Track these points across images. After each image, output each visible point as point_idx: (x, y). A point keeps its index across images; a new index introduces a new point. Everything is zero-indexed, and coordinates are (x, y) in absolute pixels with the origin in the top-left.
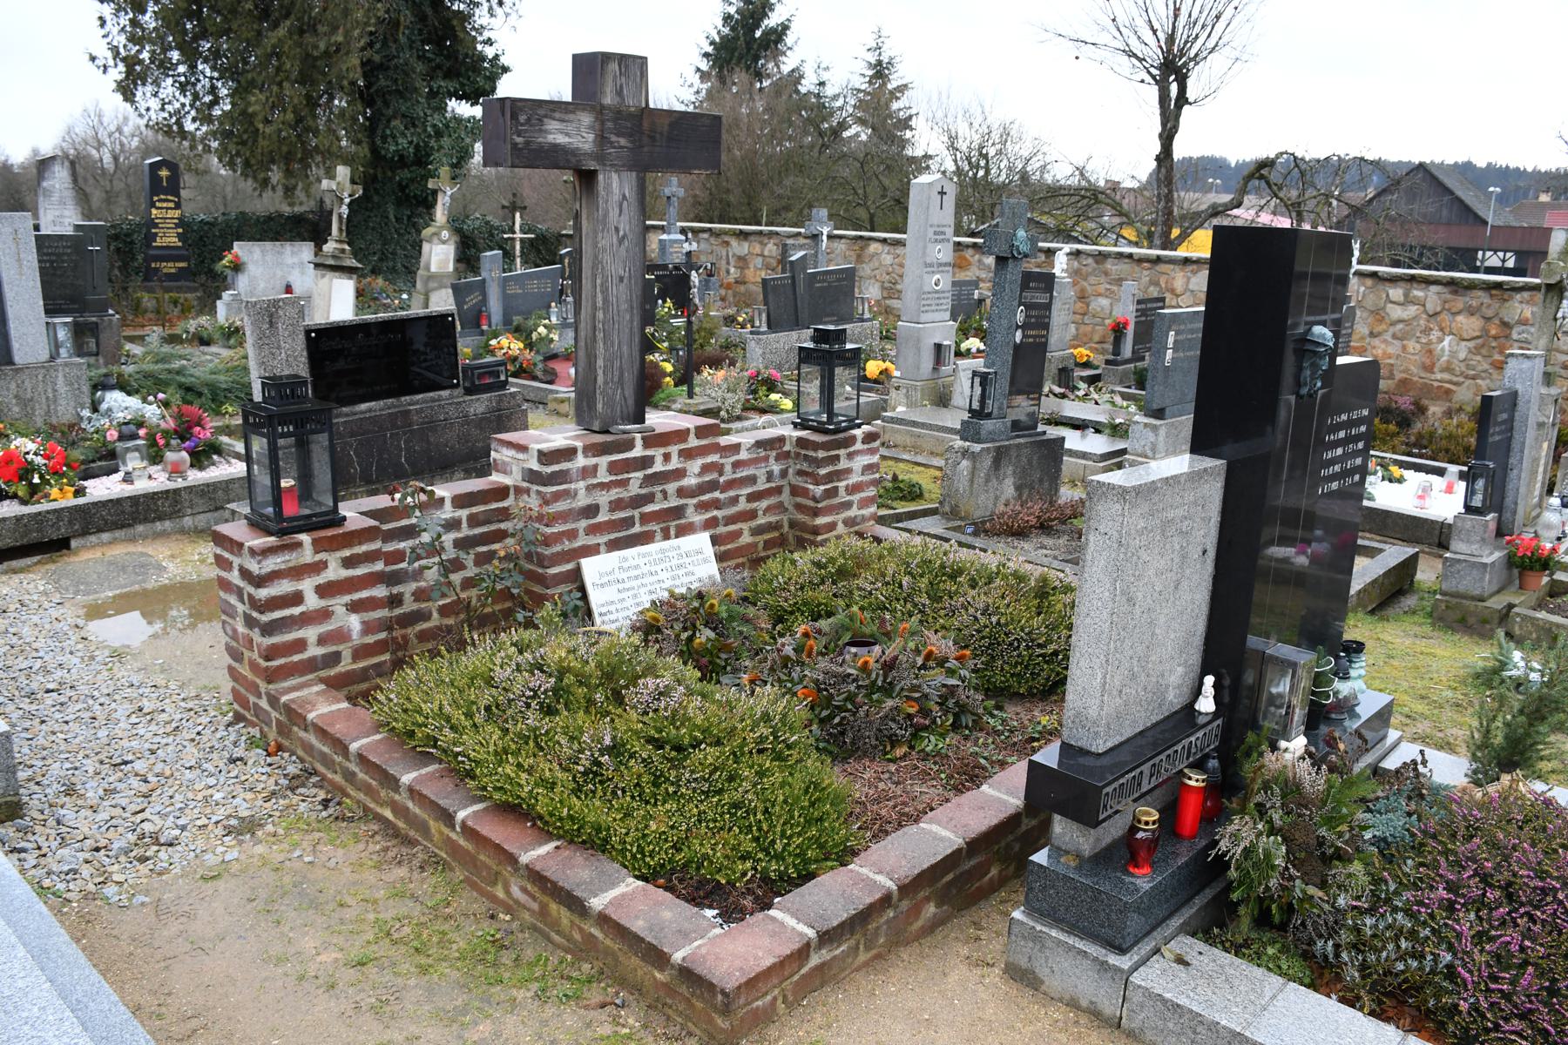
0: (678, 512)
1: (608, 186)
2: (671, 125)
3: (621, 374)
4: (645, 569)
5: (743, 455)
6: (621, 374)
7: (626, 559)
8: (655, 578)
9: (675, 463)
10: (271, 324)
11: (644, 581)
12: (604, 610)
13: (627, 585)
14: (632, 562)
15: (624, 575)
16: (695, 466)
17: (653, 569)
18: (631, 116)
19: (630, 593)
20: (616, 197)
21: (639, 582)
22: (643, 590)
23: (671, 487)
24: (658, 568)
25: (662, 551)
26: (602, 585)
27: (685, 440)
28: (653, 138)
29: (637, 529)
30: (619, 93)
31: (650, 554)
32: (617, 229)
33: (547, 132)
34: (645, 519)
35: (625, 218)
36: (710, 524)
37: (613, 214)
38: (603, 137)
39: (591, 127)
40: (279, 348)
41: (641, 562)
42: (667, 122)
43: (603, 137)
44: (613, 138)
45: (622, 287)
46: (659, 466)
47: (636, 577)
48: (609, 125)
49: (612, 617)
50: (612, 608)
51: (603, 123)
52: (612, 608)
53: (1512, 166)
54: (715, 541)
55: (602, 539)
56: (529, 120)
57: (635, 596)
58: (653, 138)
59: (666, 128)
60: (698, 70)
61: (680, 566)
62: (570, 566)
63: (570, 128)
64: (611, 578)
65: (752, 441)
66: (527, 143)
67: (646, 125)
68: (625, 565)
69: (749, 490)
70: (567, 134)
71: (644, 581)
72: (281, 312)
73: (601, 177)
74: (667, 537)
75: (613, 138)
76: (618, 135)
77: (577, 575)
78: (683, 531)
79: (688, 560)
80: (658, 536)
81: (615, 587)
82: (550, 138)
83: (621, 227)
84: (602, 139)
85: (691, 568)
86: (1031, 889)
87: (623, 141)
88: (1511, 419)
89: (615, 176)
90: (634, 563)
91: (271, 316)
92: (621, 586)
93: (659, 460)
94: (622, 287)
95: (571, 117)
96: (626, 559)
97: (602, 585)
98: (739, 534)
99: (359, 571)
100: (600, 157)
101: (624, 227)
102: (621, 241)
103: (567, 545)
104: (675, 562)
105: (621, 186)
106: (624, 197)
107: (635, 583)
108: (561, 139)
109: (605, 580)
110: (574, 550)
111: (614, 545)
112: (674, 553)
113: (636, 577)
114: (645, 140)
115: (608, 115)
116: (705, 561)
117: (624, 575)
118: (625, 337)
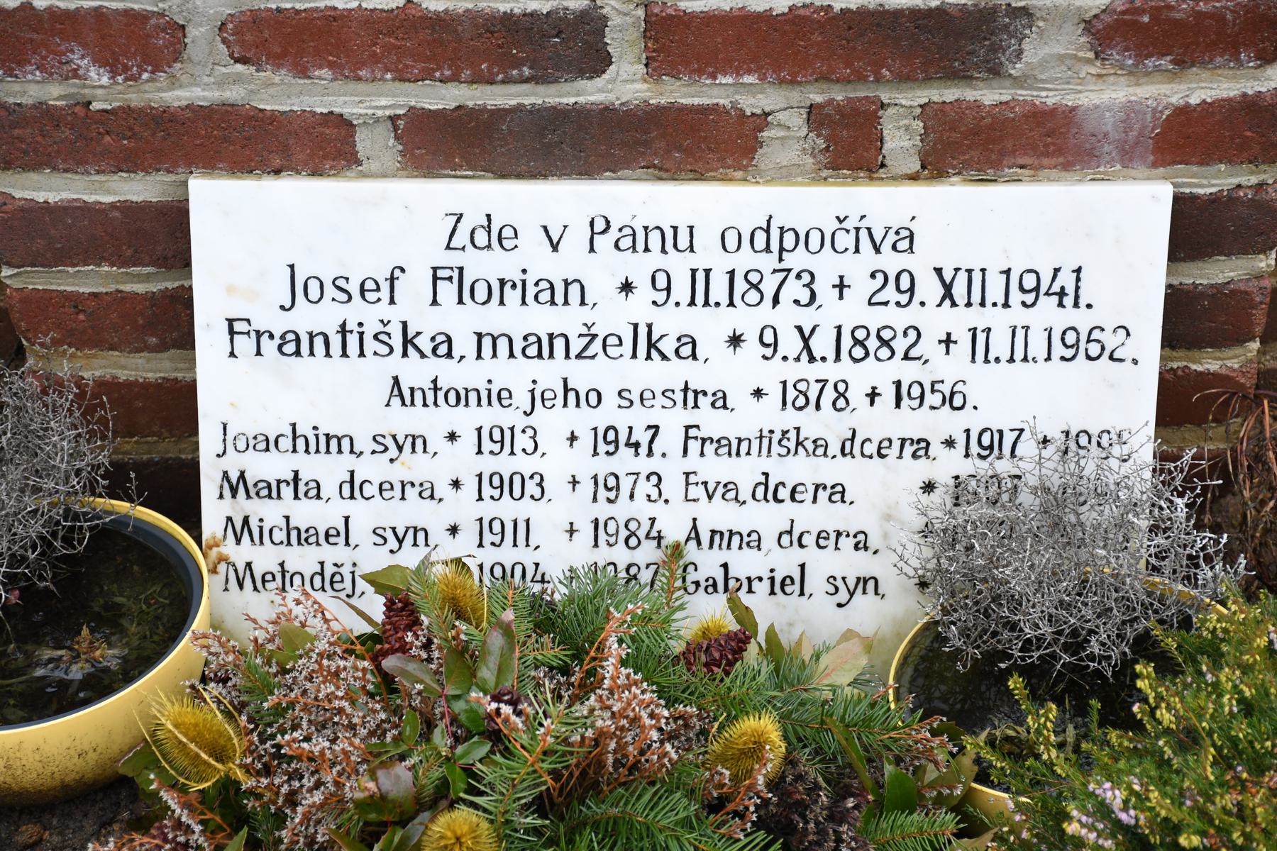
4: (614, 315)
8: (674, 373)
11: (583, 375)
13: (452, 375)
15: (461, 321)
19: (467, 419)
21: (549, 373)
24: (710, 326)
26: (292, 345)
29: (625, 83)
31: (675, 238)
41: (602, 271)
47: (542, 347)
49: (306, 513)
52: (328, 470)
53: (853, 7)
54: (1193, 230)
55: (371, 101)
61: (857, 344)
62: (139, 189)
64: (368, 315)
68: (484, 266)
71: (583, 375)
77: (167, 237)
80: (789, 135)
81: (376, 371)
86: (1105, 767)
88: (800, 83)
92: (416, 372)
96: (499, 237)
103: (101, 88)
107: (517, 375)
109: (325, 317)
110: (163, 119)
111: (438, 145)
112: (858, 267)
113: (542, 347)
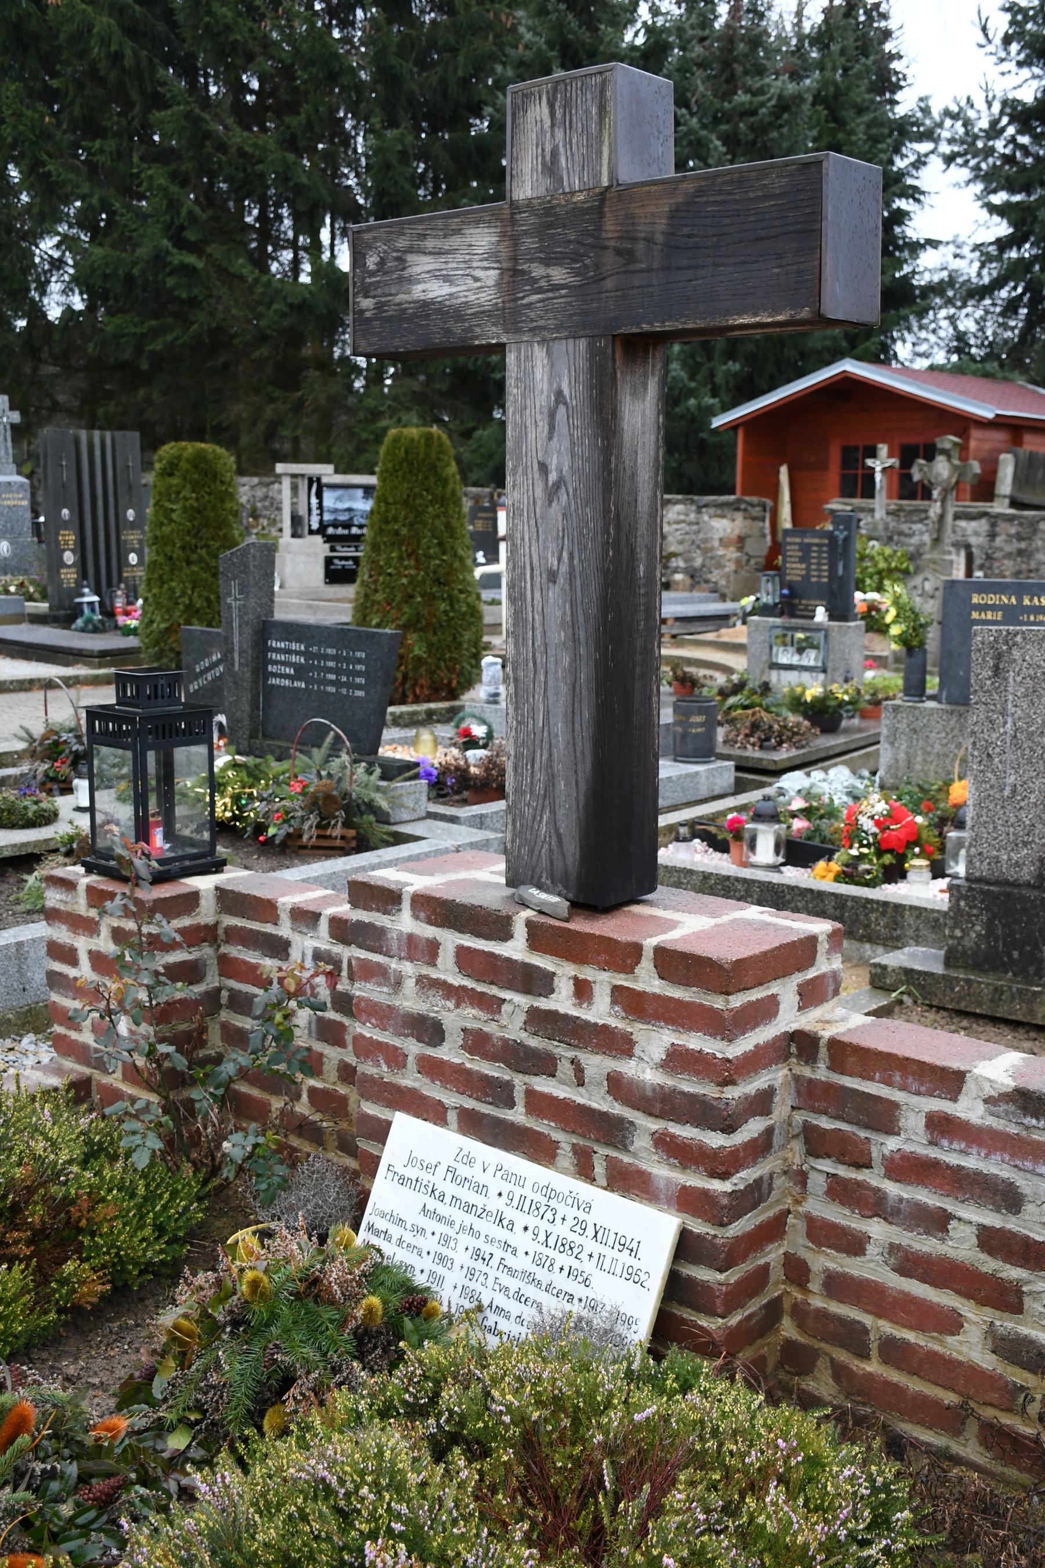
0: (613, 1131)
1: (527, 375)
2: (674, 214)
3: (551, 778)
4: (495, 1204)
5: (968, 1108)
6: (551, 778)
7: (470, 1162)
9: (600, 1011)
10: (997, 670)
11: (479, 1225)
12: (381, 1224)
13: (443, 1210)
14: (475, 1173)
15: (450, 1189)
16: (656, 1041)
17: (509, 1214)
18: (578, 212)
19: (441, 1228)
20: (542, 399)
21: (468, 1219)
22: (465, 1240)
23: (597, 1064)
24: (521, 1220)
25: (550, 1193)
27: (629, 969)
28: (627, 255)
30: (550, 168)
31: (520, 1181)
32: (543, 468)
33: (411, 281)
34: (538, 1103)
35: (561, 443)
36: (688, 1201)
37: (536, 433)
38: (515, 272)
39: (493, 256)
40: (1004, 713)
41: (496, 1185)
42: (664, 207)
43: (515, 272)
44: (538, 271)
45: (554, 593)
46: (562, 1001)
47: (469, 1208)
48: (529, 243)
50: (395, 1231)
51: (515, 241)
52: (395, 1231)
55: (451, 1099)
56: (382, 262)
57: (445, 1240)
58: (627, 255)
59: (662, 225)
60: (900, 57)
63: (452, 264)
64: (425, 1177)
65: (1008, 1083)
66: (379, 307)
67: (611, 227)
68: (463, 1171)
69: (992, 1219)
70: (447, 279)
71: (479, 1225)
72: (1016, 654)
73: (511, 358)
74: (584, 1171)
75: (538, 271)
76: (547, 262)
78: (627, 1182)
79: (591, 1246)
82: (418, 292)
83: (553, 463)
84: (513, 277)
85: (588, 1267)
87: (558, 274)
89: (539, 353)
90: (481, 1178)
91: (999, 657)
92: (432, 1204)
93: (564, 988)
94: (554, 593)
95: (455, 241)
97: (403, 1180)
98: (952, 1323)
99: (689, 1085)
100: (510, 315)
101: (559, 462)
102: (552, 492)
104: (561, 1230)
105: (553, 374)
106: (559, 393)
108: (436, 290)
109: (412, 1173)
111: (473, 1125)
112: (571, 1213)
113: (469, 1208)
114: (610, 260)
115: (527, 221)
116: (632, 1276)
117: (450, 1189)
118: (559, 705)
